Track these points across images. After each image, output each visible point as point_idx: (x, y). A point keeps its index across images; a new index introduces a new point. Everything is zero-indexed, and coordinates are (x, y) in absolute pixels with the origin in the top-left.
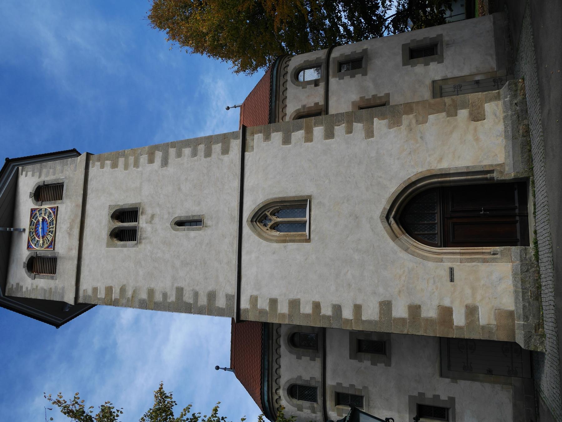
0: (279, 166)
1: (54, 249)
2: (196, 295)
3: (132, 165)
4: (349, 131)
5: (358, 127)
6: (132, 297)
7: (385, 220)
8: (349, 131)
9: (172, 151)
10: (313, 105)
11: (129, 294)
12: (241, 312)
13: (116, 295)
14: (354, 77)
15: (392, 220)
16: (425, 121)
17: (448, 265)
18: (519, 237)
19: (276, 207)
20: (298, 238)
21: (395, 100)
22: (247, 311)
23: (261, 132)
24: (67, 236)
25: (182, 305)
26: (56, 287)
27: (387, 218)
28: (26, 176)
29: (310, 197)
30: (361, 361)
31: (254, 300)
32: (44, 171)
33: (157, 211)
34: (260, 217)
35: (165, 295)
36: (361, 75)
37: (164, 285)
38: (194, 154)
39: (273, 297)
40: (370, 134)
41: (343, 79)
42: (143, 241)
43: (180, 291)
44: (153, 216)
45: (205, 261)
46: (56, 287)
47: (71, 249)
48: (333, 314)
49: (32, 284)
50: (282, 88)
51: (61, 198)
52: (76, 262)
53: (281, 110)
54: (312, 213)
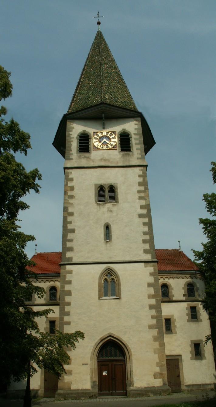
0: (137, 280)
1: (93, 150)
2: (71, 240)
3: (140, 196)
4: (152, 317)
5: (154, 321)
6: (69, 203)
7: (109, 335)
8: (152, 317)
9: (146, 220)
10: (173, 294)
11: (71, 201)
12: (64, 266)
13: (70, 193)
14: (187, 315)
15: (110, 338)
16: (155, 353)
17: (89, 363)
18: (102, 392)
19: (116, 281)
20: (113, 272)
21: (167, 338)
22: (65, 268)
23: (154, 271)
24: (101, 158)
25: (66, 231)
26: (72, 154)
27: (110, 336)
28: (135, 124)
29: (120, 298)
30: (46, 322)
31: (70, 272)
32: (137, 137)
33: (114, 214)
34: (109, 272)
35: (70, 222)
36: (188, 319)
37: (76, 222)
38: (145, 233)
39: (72, 282)
40: (150, 327)
41: (186, 310)
42: (98, 207)
43: (73, 231)
44: (111, 211)
45: (87, 244)
46: (72, 154)
47: (93, 162)
48: (66, 312)
49: (73, 138)
50: (183, 276)
51: (122, 150)
52: (86, 166)
53: (171, 276)
54: (113, 300)
